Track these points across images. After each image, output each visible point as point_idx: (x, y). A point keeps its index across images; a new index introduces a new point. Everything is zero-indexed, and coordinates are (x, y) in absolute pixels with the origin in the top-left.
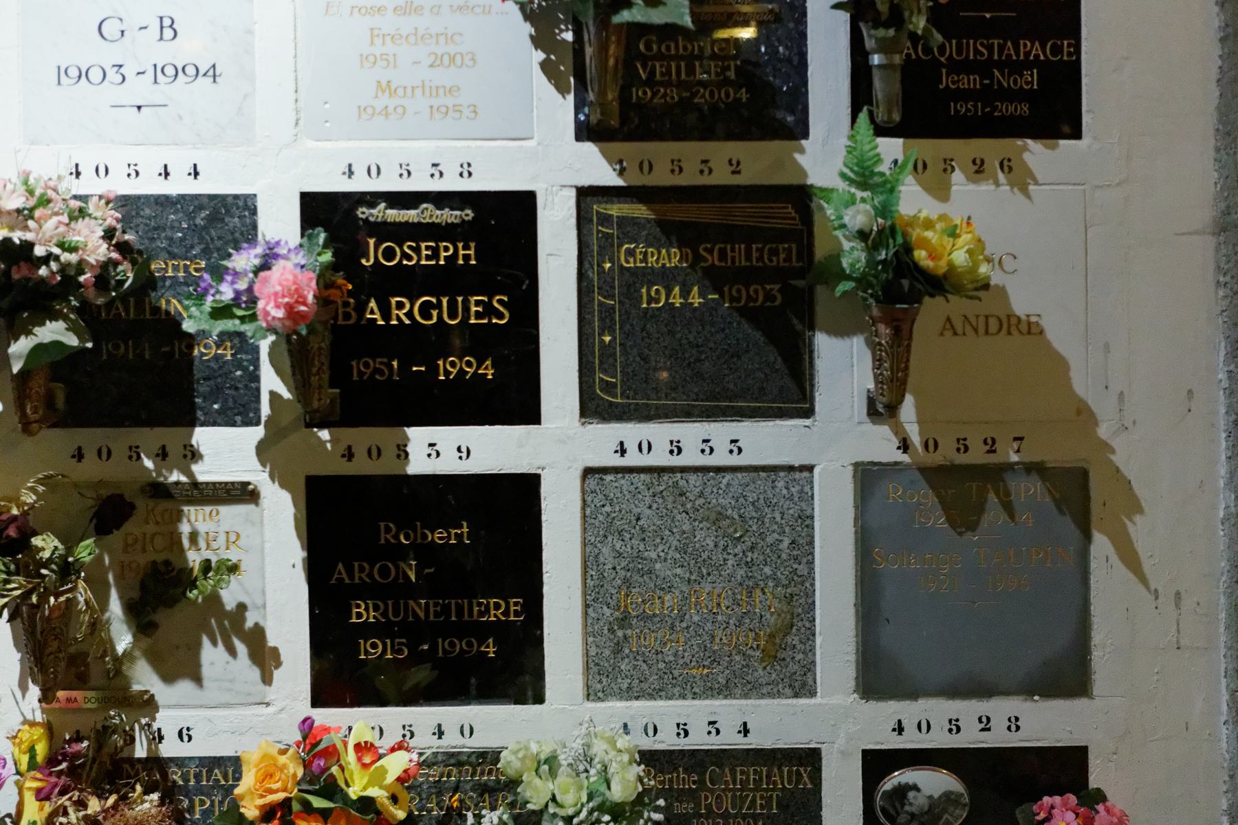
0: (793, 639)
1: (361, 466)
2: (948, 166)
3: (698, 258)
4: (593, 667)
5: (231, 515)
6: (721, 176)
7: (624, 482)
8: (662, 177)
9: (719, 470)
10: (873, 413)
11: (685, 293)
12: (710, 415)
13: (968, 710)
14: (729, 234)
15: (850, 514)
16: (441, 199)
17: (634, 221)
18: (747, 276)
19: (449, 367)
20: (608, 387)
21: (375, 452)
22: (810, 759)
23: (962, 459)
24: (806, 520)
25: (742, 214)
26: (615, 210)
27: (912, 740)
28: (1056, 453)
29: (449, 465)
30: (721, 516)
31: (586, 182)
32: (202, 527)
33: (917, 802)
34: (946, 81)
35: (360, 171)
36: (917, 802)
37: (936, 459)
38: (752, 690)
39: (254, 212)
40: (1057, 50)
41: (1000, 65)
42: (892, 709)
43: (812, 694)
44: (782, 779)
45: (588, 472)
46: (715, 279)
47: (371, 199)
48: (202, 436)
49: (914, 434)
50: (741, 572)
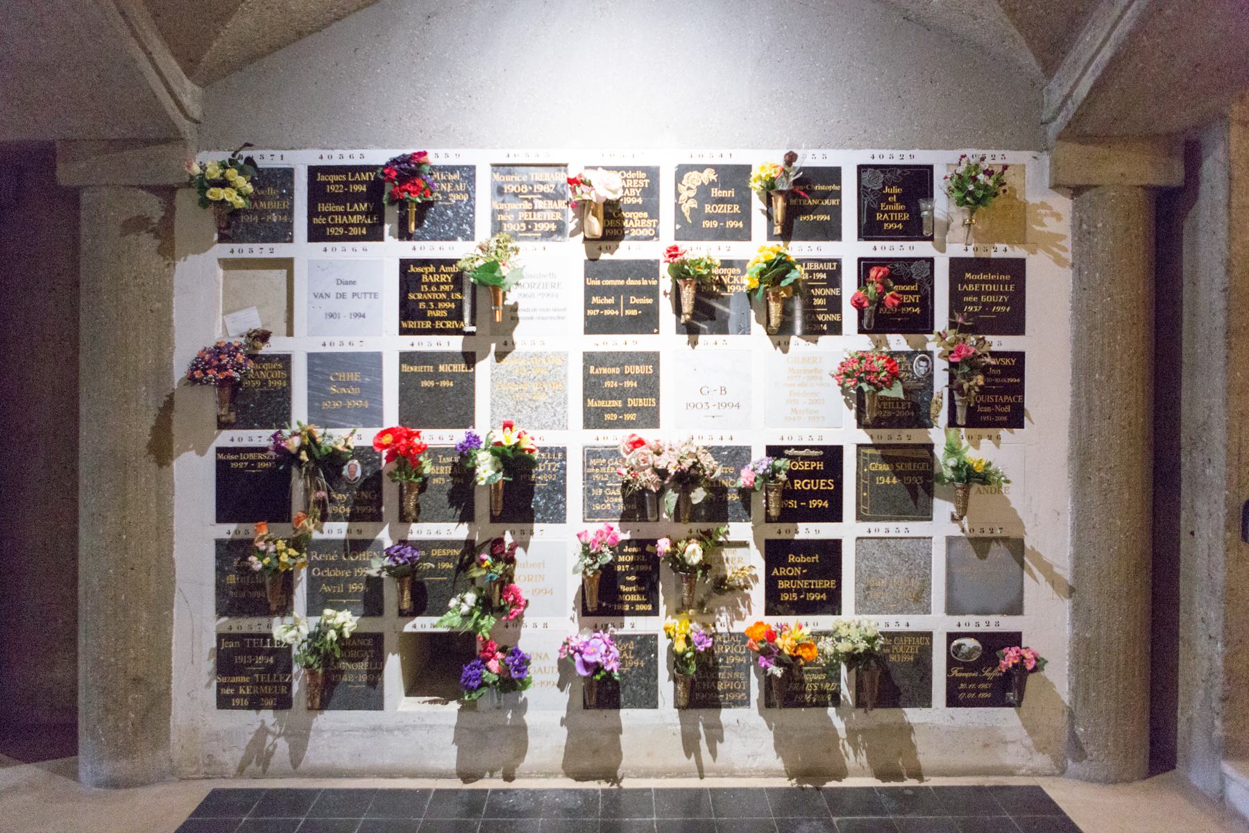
0: (924, 595)
1: (784, 536)
2: (980, 437)
3: (895, 467)
4: (858, 603)
5: (740, 551)
6: (904, 441)
7: (869, 542)
8: (884, 441)
9: (901, 538)
10: (953, 519)
11: (891, 479)
12: (897, 520)
13: (982, 619)
14: (905, 460)
15: (944, 553)
16: (812, 448)
17: (875, 455)
18: (911, 474)
19: (813, 503)
20: (865, 511)
21: (788, 531)
22: (929, 635)
23: (273, 152)
24: (929, 555)
25: (908, 453)
26: (869, 451)
27: (963, 629)
28: (1013, 533)
29: (812, 536)
30: (901, 554)
31: (860, 442)
32: (730, 556)
33: (965, 649)
34: (980, 409)
35: (785, 438)
36: (965, 649)
37: (972, 535)
38: (910, 612)
39: (750, 451)
40: (1017, 399)
41: (998, 404)
42: (957, 618)
43: (930, 613)
44: (919, 641)
45: (858, 538)
46: (899, 475)
47: (789, 448)
48: (343, 536)
49: (966, 527)
50: (907, 573)
